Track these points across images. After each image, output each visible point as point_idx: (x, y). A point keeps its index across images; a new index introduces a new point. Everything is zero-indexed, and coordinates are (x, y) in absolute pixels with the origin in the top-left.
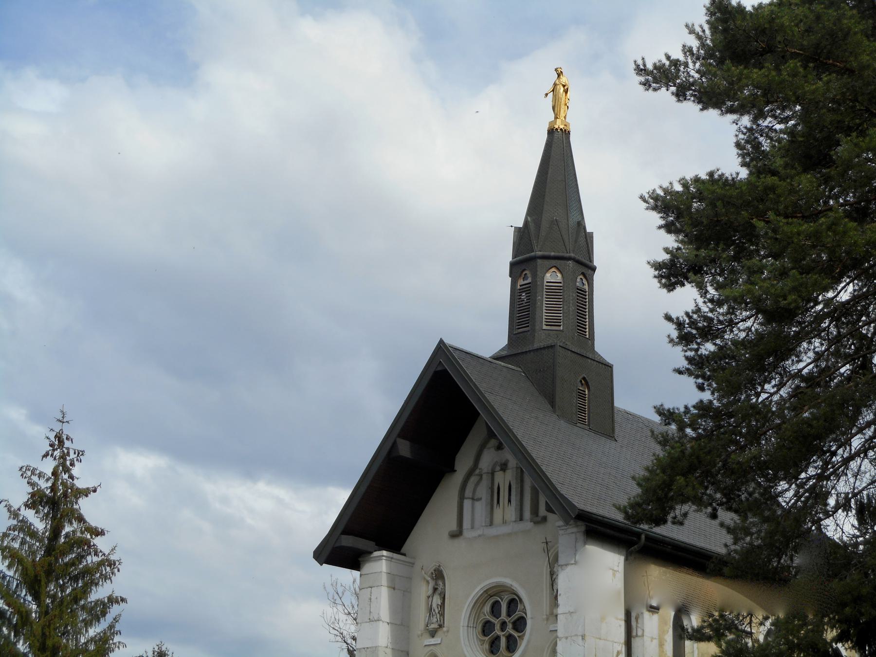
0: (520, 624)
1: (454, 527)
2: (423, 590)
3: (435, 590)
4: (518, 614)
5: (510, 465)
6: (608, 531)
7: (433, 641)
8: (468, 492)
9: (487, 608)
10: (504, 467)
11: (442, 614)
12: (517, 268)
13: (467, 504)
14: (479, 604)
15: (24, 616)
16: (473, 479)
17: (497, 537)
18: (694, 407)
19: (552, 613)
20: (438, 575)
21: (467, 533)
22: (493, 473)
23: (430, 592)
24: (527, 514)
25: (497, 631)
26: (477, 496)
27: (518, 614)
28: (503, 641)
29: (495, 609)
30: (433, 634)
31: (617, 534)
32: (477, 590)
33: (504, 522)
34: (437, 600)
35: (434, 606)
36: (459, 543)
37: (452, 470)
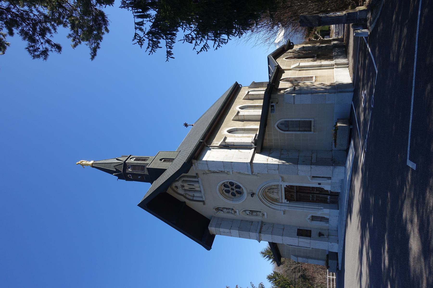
0: (232, 184)
1: (202, 203)
2: (221, 214)
3: (222, 211)
4: (228, 184)
5: (182, 184)
6: (225, 106)
7: (238, 212)
8: (191, 198)
9: (227, 194)
10: (183, 186)
11: (229, 209)
12: (128, 179)
13: (195, 199)
14: (226, 197)
15: (46, 17)
16: (187, 196)
17: (204, 190)
18: (149, 9)
19: (227, 173)
20: (218, 209)
21: (204, 200)
22: (185, 190)
23: (222, 212)
24: (196, 180)
25: (234, 191)
26: (192, 195)
27: (228, 184)
28: (237, 190)
29: (228, 192)
30: (235, 212)
31: (225, 106)
32: (221, 197)
33: (200, 187)
34: (225, 210)
35: (227, 211)
36: (206, 202)
37: (184, 203)
